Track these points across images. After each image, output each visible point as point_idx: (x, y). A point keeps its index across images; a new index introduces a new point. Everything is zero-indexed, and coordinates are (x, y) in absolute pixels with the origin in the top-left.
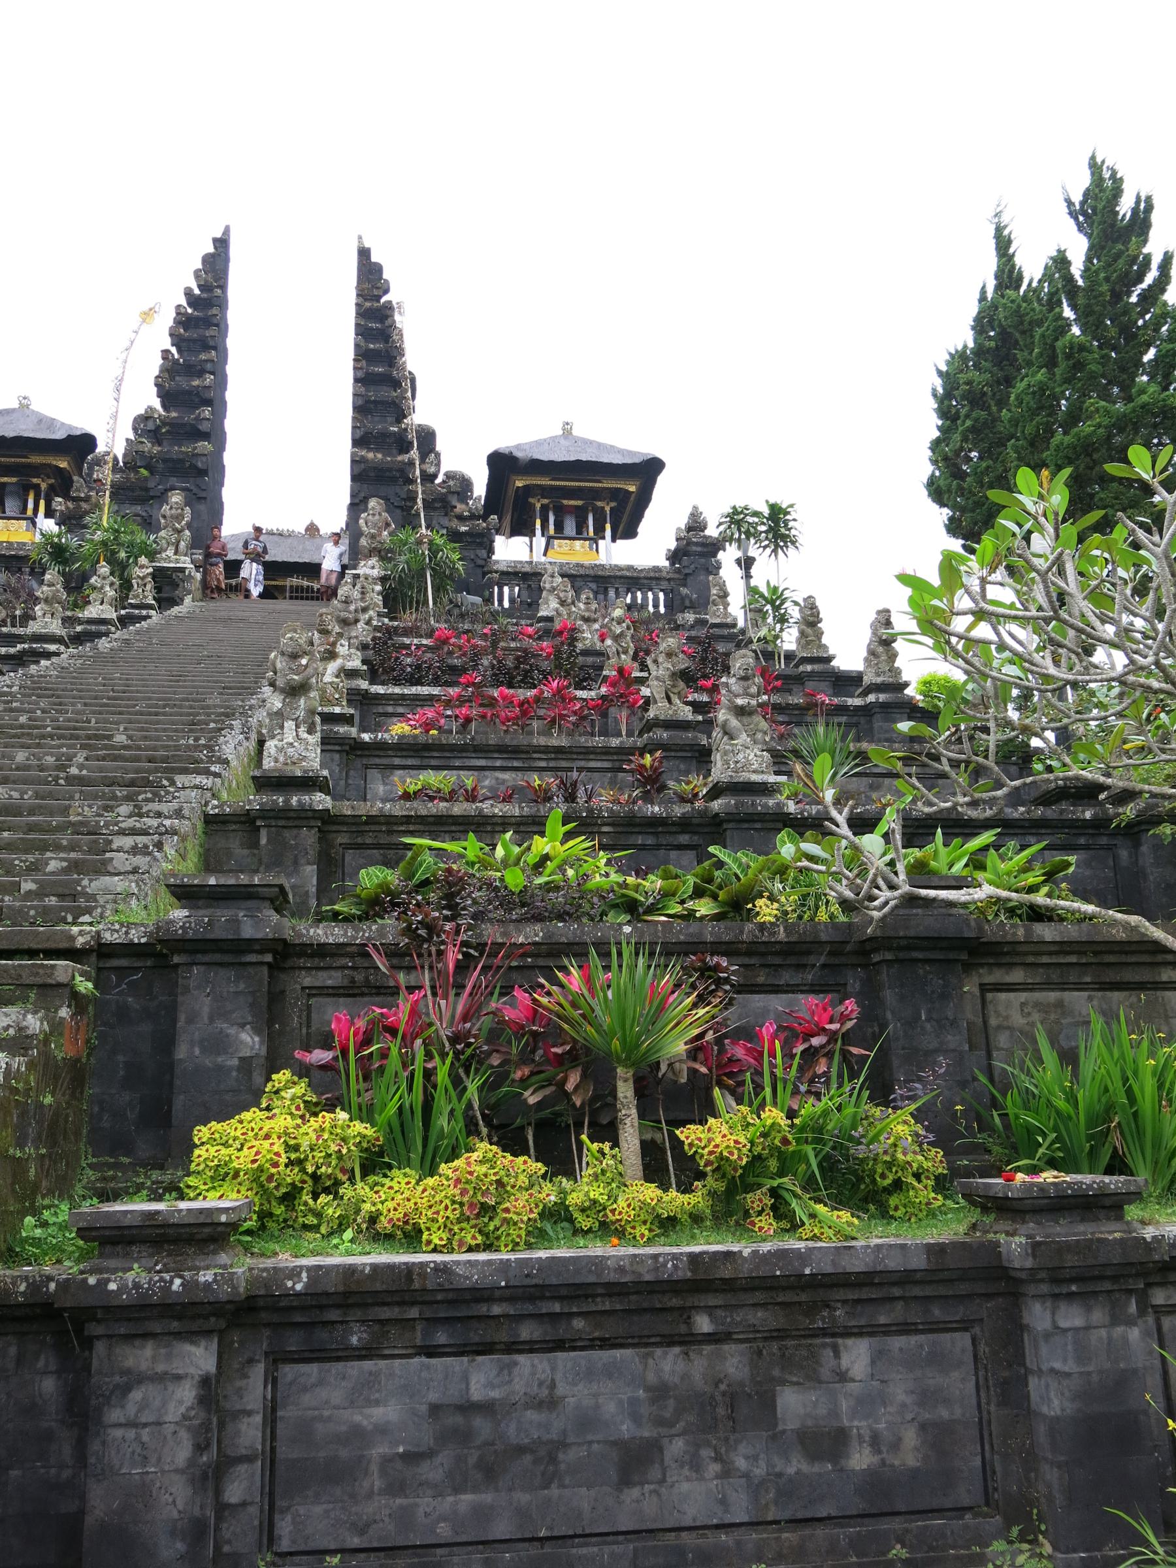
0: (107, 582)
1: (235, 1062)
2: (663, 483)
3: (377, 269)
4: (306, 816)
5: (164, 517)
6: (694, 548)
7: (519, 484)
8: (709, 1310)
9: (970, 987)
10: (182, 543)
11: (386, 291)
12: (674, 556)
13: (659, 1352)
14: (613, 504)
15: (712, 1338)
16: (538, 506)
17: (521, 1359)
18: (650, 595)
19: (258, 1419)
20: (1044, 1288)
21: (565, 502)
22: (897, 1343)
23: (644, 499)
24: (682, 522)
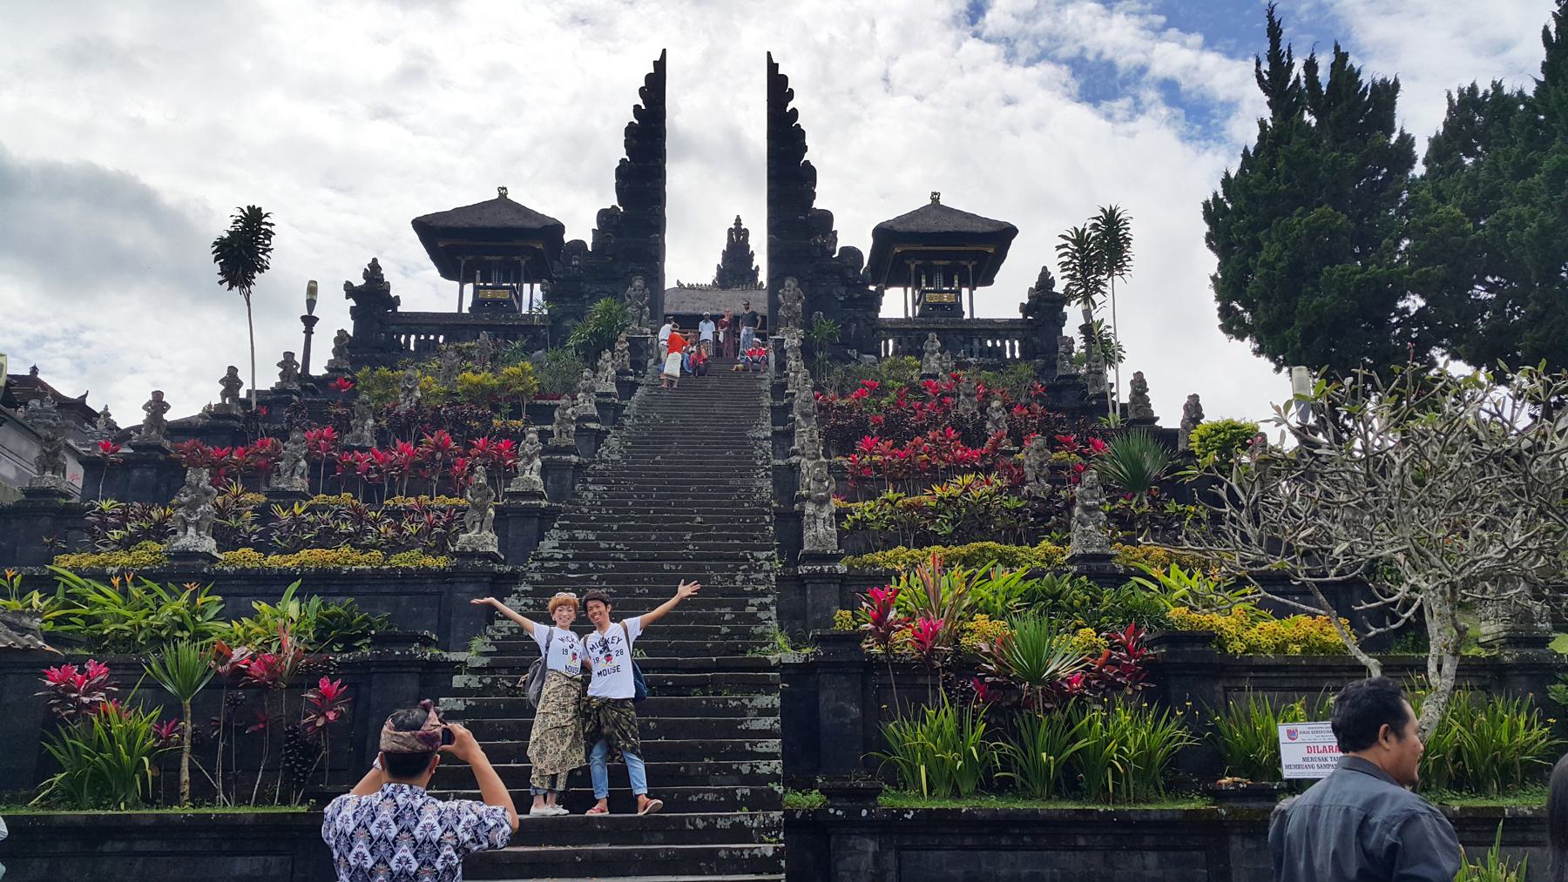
0: (610, 364)
1: (848, 721)
2: (1016, 247)
3: (785, 79)
4: (832, 577)
5: (629, 296)
6: (1043, 304)
7: (898, 250)
8: (1085, 836)
9: (1219, 688)
10: (644, 317)
11: (791, 97)
12: (1025, 309)
13: (1063, 853)
14: (974, 263)
15: (1083, 849)
16: (913, 267)
17: (1003, 853)
18: (1007, 343)
19: (894, 873)
20: (1238, 830)
21: (935, 262)
22: (1171, 854)
23: (1001, 256)
24: (1032, 282)
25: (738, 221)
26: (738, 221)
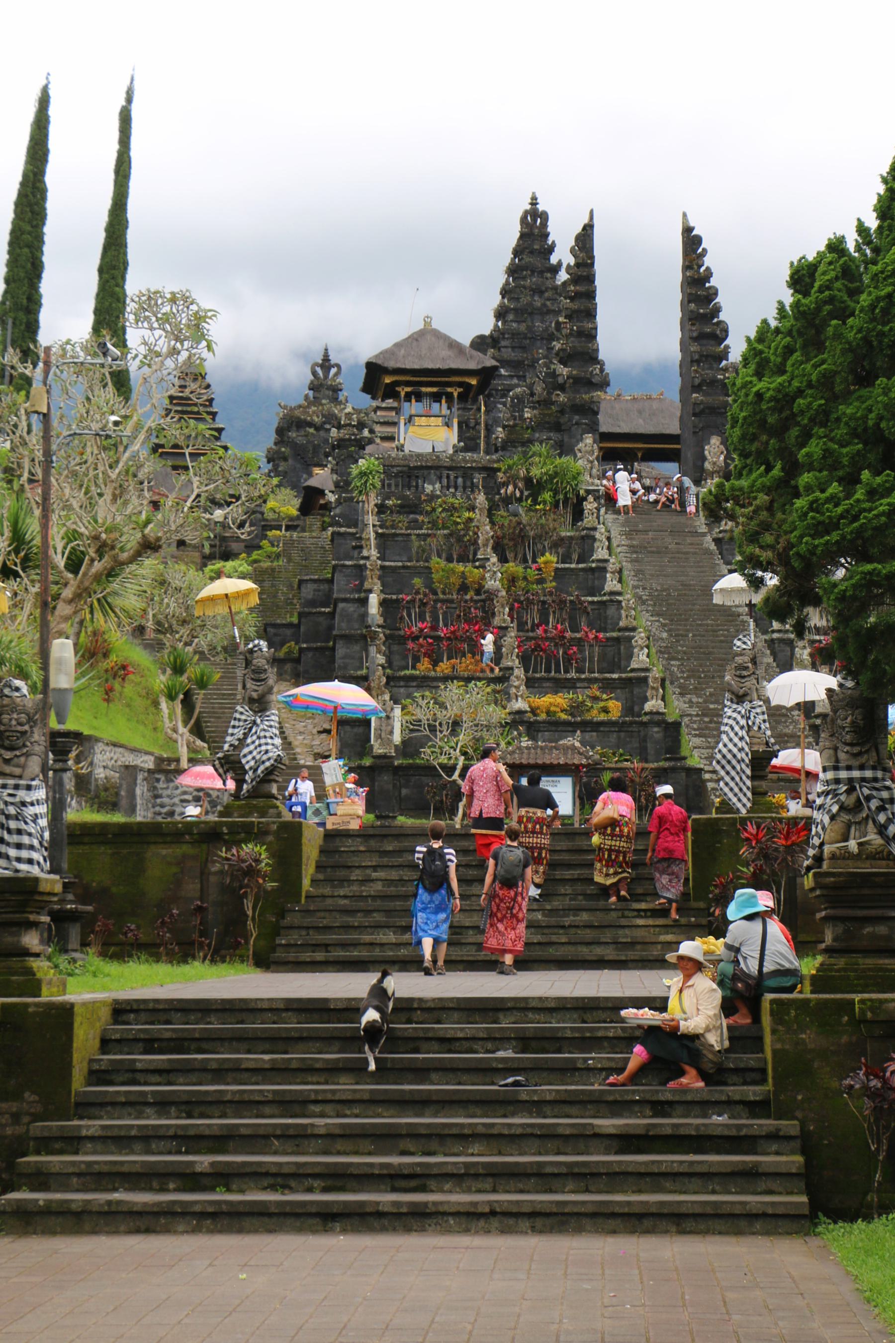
3: (698, 240)
25: (534, 202)
26: (534, 202)
